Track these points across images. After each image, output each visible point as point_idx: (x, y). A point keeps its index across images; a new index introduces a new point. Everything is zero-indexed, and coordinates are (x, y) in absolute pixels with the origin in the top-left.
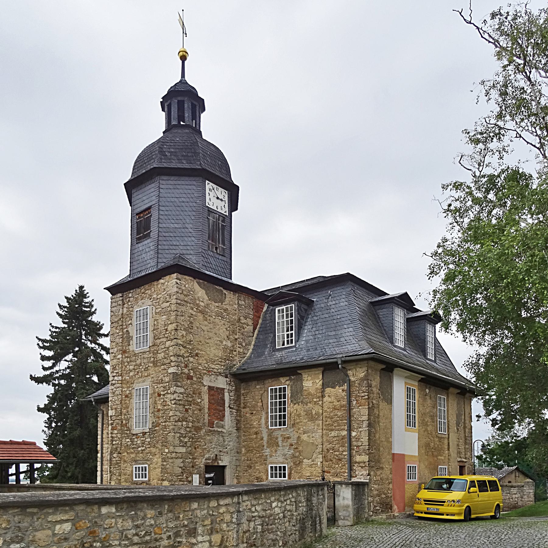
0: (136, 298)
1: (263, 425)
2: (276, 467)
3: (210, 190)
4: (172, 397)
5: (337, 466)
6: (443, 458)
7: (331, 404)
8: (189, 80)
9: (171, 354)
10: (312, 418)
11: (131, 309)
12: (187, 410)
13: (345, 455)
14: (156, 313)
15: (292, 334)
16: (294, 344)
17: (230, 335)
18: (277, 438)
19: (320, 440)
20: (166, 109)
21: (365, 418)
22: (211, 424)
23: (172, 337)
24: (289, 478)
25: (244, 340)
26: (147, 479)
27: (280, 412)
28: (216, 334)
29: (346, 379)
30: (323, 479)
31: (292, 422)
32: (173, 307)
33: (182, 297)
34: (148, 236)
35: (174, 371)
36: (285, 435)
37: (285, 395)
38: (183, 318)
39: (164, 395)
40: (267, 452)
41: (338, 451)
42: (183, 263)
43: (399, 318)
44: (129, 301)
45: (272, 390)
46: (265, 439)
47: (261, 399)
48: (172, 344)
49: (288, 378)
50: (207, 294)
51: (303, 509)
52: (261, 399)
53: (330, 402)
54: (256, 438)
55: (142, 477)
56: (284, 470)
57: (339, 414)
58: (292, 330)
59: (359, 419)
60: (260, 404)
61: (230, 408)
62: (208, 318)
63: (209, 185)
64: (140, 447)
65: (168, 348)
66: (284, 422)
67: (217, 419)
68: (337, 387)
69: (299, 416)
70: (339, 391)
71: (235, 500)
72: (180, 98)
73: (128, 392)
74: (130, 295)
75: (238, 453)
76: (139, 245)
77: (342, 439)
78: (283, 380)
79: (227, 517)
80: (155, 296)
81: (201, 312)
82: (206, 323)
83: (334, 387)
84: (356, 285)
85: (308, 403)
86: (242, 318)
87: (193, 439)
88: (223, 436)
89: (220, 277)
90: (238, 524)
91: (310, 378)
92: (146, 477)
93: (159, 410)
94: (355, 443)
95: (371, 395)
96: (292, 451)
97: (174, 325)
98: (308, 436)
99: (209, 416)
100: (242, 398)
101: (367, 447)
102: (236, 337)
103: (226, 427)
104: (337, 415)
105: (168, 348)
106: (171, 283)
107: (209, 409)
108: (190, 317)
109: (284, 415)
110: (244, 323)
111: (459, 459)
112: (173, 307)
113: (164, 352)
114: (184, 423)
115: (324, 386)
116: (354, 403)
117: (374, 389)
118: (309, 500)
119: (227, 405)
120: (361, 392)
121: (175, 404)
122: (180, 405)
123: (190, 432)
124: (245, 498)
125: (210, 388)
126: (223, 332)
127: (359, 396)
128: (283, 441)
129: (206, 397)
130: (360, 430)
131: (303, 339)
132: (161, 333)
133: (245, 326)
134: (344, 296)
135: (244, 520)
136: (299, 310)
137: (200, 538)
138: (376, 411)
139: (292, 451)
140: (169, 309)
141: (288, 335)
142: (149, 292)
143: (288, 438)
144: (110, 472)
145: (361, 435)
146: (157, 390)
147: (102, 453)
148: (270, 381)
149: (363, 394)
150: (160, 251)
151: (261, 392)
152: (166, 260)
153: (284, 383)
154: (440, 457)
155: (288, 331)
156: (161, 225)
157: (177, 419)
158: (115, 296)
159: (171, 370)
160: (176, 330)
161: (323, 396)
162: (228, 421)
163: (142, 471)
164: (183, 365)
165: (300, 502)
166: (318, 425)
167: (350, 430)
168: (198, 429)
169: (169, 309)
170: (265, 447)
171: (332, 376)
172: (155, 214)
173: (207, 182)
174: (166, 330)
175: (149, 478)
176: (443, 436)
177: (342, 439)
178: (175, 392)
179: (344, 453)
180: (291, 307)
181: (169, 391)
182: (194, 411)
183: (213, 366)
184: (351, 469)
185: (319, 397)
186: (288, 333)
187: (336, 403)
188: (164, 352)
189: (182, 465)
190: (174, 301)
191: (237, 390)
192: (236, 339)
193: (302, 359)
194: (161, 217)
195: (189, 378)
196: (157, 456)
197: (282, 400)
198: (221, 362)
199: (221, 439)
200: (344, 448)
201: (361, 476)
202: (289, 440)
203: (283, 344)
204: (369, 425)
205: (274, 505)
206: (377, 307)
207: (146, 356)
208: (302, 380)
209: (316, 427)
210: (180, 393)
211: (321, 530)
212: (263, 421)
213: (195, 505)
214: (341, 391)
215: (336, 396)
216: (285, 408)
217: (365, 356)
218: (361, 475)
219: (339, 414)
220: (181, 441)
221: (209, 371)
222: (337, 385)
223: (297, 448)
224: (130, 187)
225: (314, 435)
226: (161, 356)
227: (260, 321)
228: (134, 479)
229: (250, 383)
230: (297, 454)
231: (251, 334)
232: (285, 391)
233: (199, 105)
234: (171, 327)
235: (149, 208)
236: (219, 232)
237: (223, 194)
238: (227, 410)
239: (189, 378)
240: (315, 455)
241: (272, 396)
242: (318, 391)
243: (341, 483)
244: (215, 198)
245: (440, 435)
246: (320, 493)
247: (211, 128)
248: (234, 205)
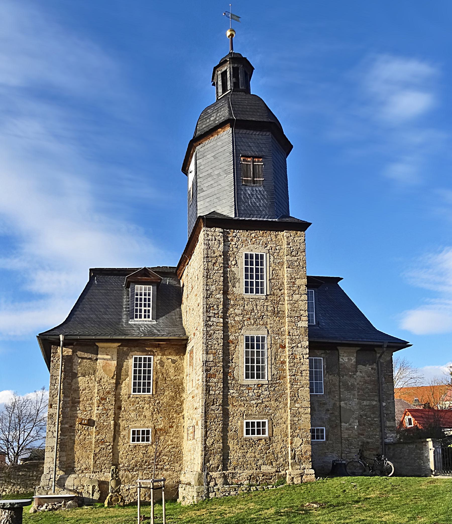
5: (369, 429)
7: (363, 379)
13: (376, 421)
24: (327, 439)
36: (321, 401)
41: (370, 417)
49: (323, 352)
53: (362, 377)
57: (370, 387)
58: (149, 306)
59: (388, 393)
68: (368, 366)
77: (373, 408)
83: (365, 365)
85: (344, 375)
91: (345, 355)
96: (329, 416)
98: (346, 404)
104: (367, 388)
130: (389, 401)
135: (334, 482)
139: (329, 416)
141: (145, 310)
166: (354, 395)
167: (380, 401)
177: (373, 408)
179: (375, 419)
185: (353, 372)
186: (145, 308)
187: (367, 378)
197: (147, 369)
200: (375, 415)
202: (325, 406)
214: (370, 369)
218: (391, 437)
219: (370, 387)
222: (367, 364)
223: (332, 413)
240: (352, 420)
242: (353, 366)
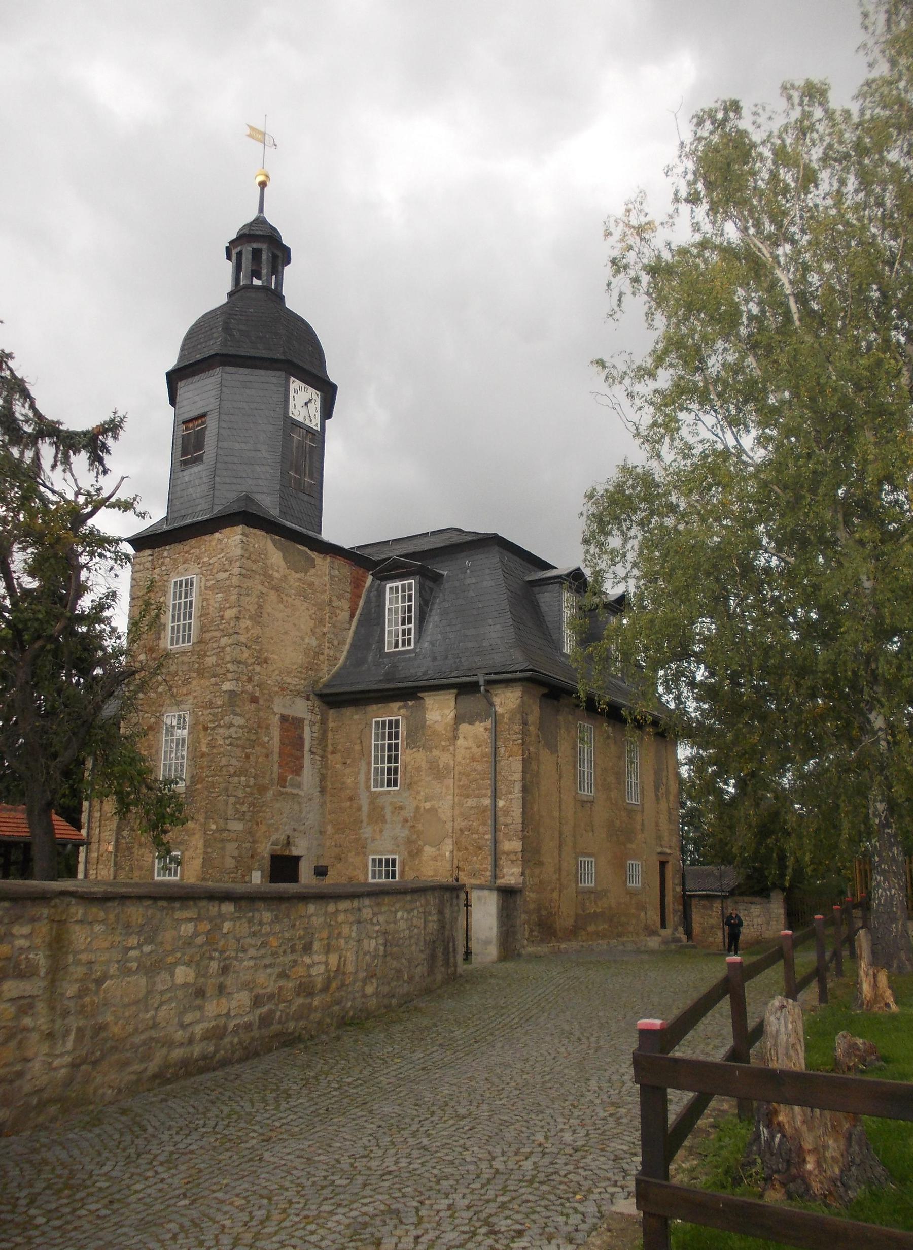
0: (175, 560)
1: (362, 785)
2: (380, 860)
3: (296, 391)
4: (227, 734)
6: (634, 846)
8: (272, 219)
9: (228, 658)
10: (438, 772)
11: (165, 578)
12: (247, 757)
14: (206, 588)
15: (410, 630)
16: (412, 647)
17: (315, 627)
18: (383, 808)
19: (449, 814)
20: (234, 258)
21: (518, 776)
22: (282, 781)
23: (231, 631)
25: (336, 635)
26: (178, 878)
27: (389, 762)
28: (295, 625)
29: (489, 711)
30: (457, 880)
31: (408, 781)
32: (235, 581)
33: (249, 564)
34: (198, 460)
35: (232, 688)
37: (397, 733)
38: (248, 599)
39: (213, 729)
40: (367, 831)
41: (477, 832)
42: (252, 510)
43: (567, 606)
44: (163, 563)
45: (377, 723)
46: (365, 809)
47: (360, 738)
48: (230, 641)
50: (284, 558)
51: (433, 926)
52: (360, 738)
54: (351, 807)
56: (394, 865)
58: (410, 622)
60: (357, 748)
61: (312, 753)
62: (285, 598)
63: (295, 384)
65: (224, 648)
66: (396, 781)
67: (292, 772)
69: (418, 769)
70: (480, 729)
71: (356, 903)
72: (255, 245)
73: (153, 720)
74: (166, 554)
75: (321, 832)
76: (185, 473)
78: (395, 705)
79: (346, 930)
80: (206, 559)
81: (273, 588)
82: (282, 606)
84: (505, 552)
86: (334, 598)
87: (255, 806)
88: (299, 803)
89: (304, 531)
90: (358, 941)
92: (175, 875)
93: (203, 755)
94: (501, 819)
95: (528, 739)
97: (235, 610)
99: (280, 766)
100: (330, 735)
101: (520, 827)
102: (325, 630)
103: (305, 788)
105: (224, 648)
106: (232, 539)
107: (280, 755)
108: (259, 597)
109: (396, 769)
110: (338, 608)
111: (659, 850)
112: (235, 581)
113: (216, 654)
114: (243, 779)
115: (459, 719)
116: (502, 750)
117: (532, 728)
118: (441, 912)
119: (307, 747)
120: (512, 734)
121: (231, 744)
122: (237, 746)
123: (251, 794)
124: (367, 901)
125: (284, 719)
126: (305, 624)
127: (509, 740)
128: (393, 813)
129: (276, 733)
130: (511, 796)
131: (427, 638)
132: (212, 622)
133: (338, 611)
134: (487, 571)
136: (421, 590)
137: (316, 958)
138: (534, 766)
140: (228, 582)
142: (196, 551)
143: (401, 808)
144: (115, 864)
145: (511, 803)
146: (201, 719)
147: (89, 828)
148: (375, 707)
149: (515, 737)
150: (217, 486)
151: (360, 726)
152: (226, 500)
153: (396, 712)
154: (629, 846)
155: (403, 623)
156: (220, 444)
157: (232, 771)
158: (141, 554)
159: (227, 686)
160: (238, 618)
161: (456, 738)
162: (309, 775)
164: (245, 678)
165: (430, 914)
166: (448, 788)
167: (495, 797)
168: (262, 789)
169: (228, 582)
170: (364, 824)
171: (472, 703)
172: (212, 425)
173: (292, 379)
174: (222, 617)
176: (635, 808)
178: (231, 725)
179: (487, 837)
180: (410, 584)
182: (257, 757)
183: (289, 680)
184: (496, 865)
188: (216, 654)
189: (236, 853)
190: (236, 571)
191: (323, 722)
192: (324, 634)
193: (425, 673)
194: (222, 431)
195: (254, 700)
196: (197, 836)
198: (301, 672)
199: (296, 807)
201: (511, 875)
202: (402, 813)
203: (396, 646)
204: (525, 789)
205: (399, 915)
206: (536, 589)
207: (186, 659)
208: (423, 709)
209: (444, 790)
210: (239, 726)
211: (455, 966)
212: (362, 777)
213: (312, 908)
214: (482, 729)
215: (476, 737)
216: (396, 757)
217: (519, 675)
219: (479, 768)
220: (237, 810)
221: (283, 690)
224: (174, 378)
225: (445, 802)
226: (211, 660)
227: (361, 603)
228: (156, 878)
229: (344, 710)
230: (415, 836)
231: (347, 626)
232: (397, 726)
233: (280, 255)
234: (229, 614)
235: (203, 416)
236: (303, 456)
237: (315, 395)
238: (307, 757)
239: (254, 700)
241: (377, 734)
243: (481, 887)
244: (302, 402)
245: (630, 807)
246: (455, 901)
247: (299, 290)
248: (327, 411)
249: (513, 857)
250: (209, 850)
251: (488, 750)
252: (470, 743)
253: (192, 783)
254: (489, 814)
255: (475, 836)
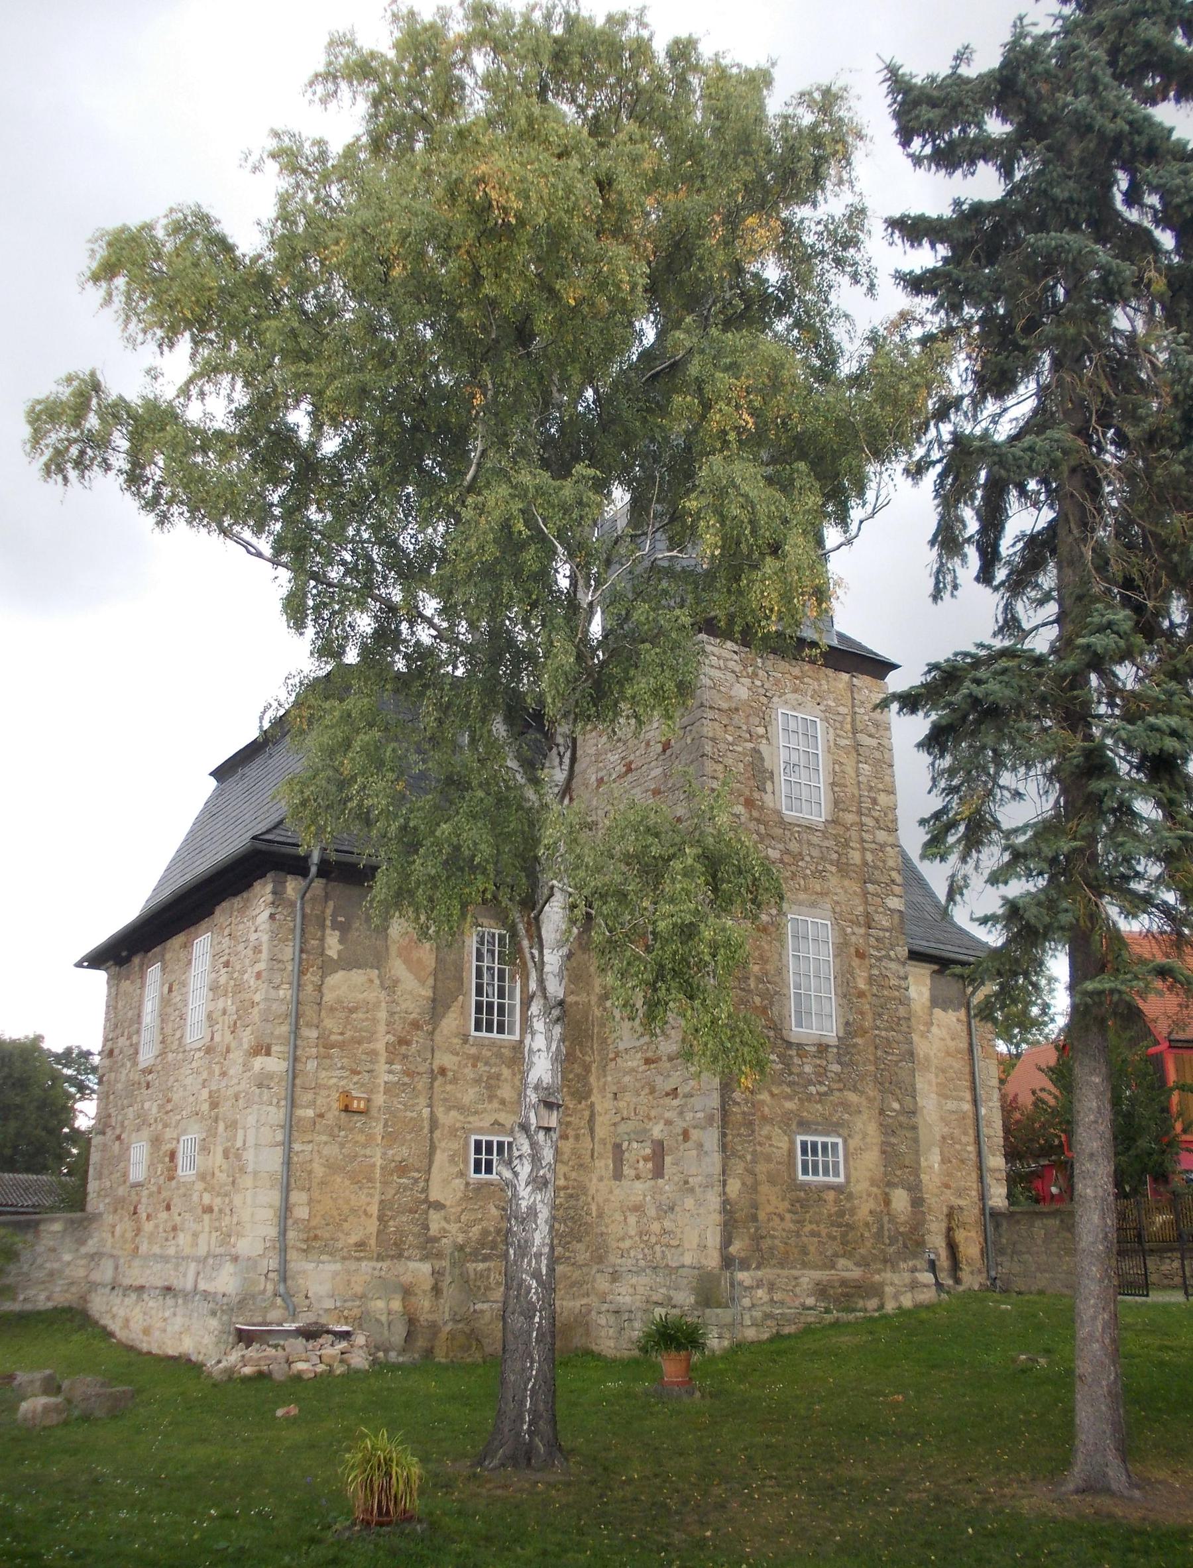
26: (841, 1179)
39: (879, 959)
55: (826, 1173)
64: (810, 1083)
138: (176, 998)
144: (724, 1147)
163: (815, 1164)
167: (975, 1102)
175: (847, 1177)
181: (892, 953)
196: (865, 1117)
228: (801, 1177)
249: (997, 1175)
250: (893, 1140)
251: (964, 1045)
252: (944, 1033)
253: (848, 1033)
254: (970, 1122)
255: (958, 1147)
